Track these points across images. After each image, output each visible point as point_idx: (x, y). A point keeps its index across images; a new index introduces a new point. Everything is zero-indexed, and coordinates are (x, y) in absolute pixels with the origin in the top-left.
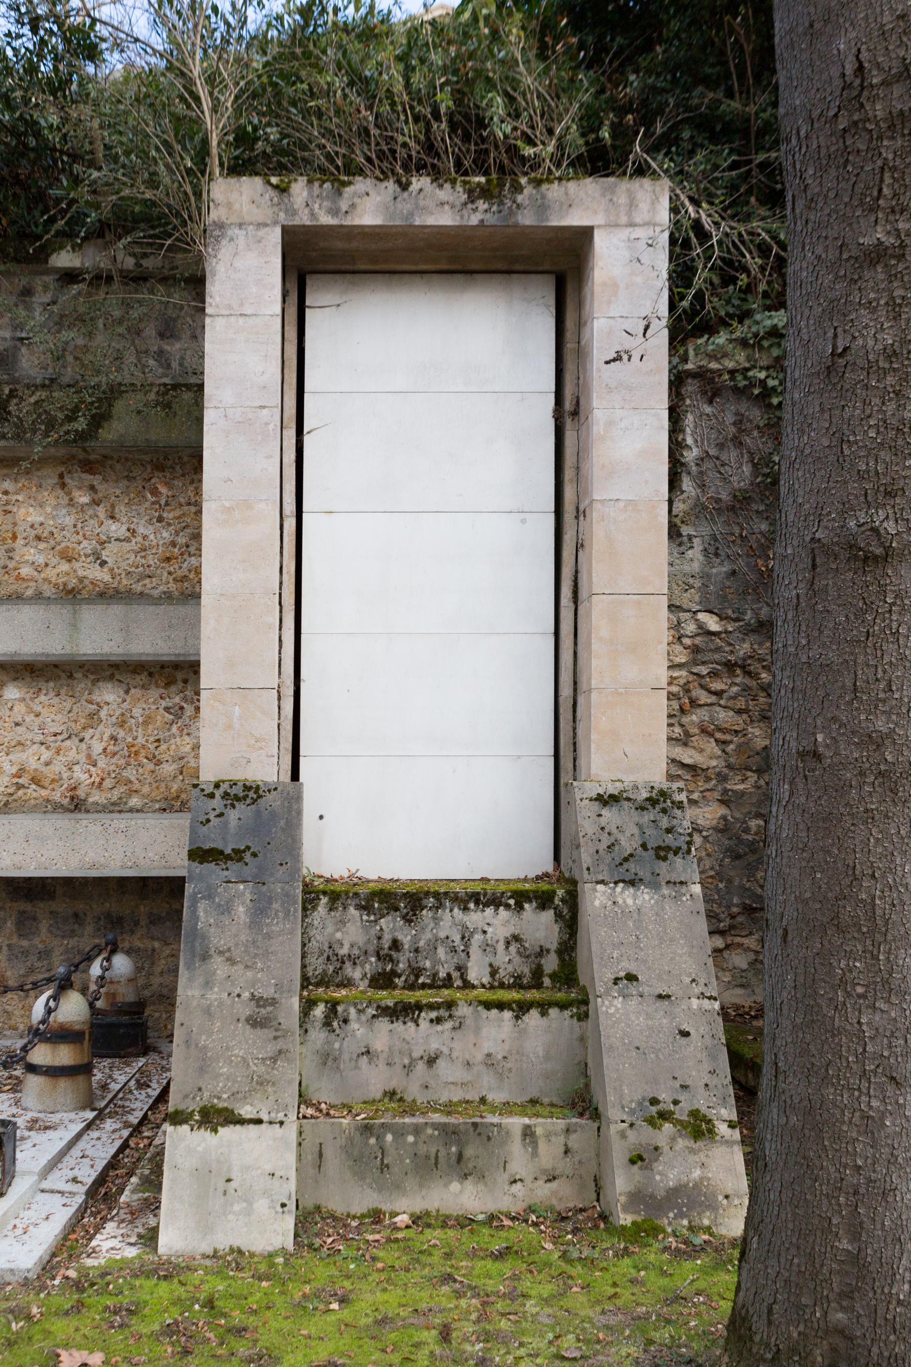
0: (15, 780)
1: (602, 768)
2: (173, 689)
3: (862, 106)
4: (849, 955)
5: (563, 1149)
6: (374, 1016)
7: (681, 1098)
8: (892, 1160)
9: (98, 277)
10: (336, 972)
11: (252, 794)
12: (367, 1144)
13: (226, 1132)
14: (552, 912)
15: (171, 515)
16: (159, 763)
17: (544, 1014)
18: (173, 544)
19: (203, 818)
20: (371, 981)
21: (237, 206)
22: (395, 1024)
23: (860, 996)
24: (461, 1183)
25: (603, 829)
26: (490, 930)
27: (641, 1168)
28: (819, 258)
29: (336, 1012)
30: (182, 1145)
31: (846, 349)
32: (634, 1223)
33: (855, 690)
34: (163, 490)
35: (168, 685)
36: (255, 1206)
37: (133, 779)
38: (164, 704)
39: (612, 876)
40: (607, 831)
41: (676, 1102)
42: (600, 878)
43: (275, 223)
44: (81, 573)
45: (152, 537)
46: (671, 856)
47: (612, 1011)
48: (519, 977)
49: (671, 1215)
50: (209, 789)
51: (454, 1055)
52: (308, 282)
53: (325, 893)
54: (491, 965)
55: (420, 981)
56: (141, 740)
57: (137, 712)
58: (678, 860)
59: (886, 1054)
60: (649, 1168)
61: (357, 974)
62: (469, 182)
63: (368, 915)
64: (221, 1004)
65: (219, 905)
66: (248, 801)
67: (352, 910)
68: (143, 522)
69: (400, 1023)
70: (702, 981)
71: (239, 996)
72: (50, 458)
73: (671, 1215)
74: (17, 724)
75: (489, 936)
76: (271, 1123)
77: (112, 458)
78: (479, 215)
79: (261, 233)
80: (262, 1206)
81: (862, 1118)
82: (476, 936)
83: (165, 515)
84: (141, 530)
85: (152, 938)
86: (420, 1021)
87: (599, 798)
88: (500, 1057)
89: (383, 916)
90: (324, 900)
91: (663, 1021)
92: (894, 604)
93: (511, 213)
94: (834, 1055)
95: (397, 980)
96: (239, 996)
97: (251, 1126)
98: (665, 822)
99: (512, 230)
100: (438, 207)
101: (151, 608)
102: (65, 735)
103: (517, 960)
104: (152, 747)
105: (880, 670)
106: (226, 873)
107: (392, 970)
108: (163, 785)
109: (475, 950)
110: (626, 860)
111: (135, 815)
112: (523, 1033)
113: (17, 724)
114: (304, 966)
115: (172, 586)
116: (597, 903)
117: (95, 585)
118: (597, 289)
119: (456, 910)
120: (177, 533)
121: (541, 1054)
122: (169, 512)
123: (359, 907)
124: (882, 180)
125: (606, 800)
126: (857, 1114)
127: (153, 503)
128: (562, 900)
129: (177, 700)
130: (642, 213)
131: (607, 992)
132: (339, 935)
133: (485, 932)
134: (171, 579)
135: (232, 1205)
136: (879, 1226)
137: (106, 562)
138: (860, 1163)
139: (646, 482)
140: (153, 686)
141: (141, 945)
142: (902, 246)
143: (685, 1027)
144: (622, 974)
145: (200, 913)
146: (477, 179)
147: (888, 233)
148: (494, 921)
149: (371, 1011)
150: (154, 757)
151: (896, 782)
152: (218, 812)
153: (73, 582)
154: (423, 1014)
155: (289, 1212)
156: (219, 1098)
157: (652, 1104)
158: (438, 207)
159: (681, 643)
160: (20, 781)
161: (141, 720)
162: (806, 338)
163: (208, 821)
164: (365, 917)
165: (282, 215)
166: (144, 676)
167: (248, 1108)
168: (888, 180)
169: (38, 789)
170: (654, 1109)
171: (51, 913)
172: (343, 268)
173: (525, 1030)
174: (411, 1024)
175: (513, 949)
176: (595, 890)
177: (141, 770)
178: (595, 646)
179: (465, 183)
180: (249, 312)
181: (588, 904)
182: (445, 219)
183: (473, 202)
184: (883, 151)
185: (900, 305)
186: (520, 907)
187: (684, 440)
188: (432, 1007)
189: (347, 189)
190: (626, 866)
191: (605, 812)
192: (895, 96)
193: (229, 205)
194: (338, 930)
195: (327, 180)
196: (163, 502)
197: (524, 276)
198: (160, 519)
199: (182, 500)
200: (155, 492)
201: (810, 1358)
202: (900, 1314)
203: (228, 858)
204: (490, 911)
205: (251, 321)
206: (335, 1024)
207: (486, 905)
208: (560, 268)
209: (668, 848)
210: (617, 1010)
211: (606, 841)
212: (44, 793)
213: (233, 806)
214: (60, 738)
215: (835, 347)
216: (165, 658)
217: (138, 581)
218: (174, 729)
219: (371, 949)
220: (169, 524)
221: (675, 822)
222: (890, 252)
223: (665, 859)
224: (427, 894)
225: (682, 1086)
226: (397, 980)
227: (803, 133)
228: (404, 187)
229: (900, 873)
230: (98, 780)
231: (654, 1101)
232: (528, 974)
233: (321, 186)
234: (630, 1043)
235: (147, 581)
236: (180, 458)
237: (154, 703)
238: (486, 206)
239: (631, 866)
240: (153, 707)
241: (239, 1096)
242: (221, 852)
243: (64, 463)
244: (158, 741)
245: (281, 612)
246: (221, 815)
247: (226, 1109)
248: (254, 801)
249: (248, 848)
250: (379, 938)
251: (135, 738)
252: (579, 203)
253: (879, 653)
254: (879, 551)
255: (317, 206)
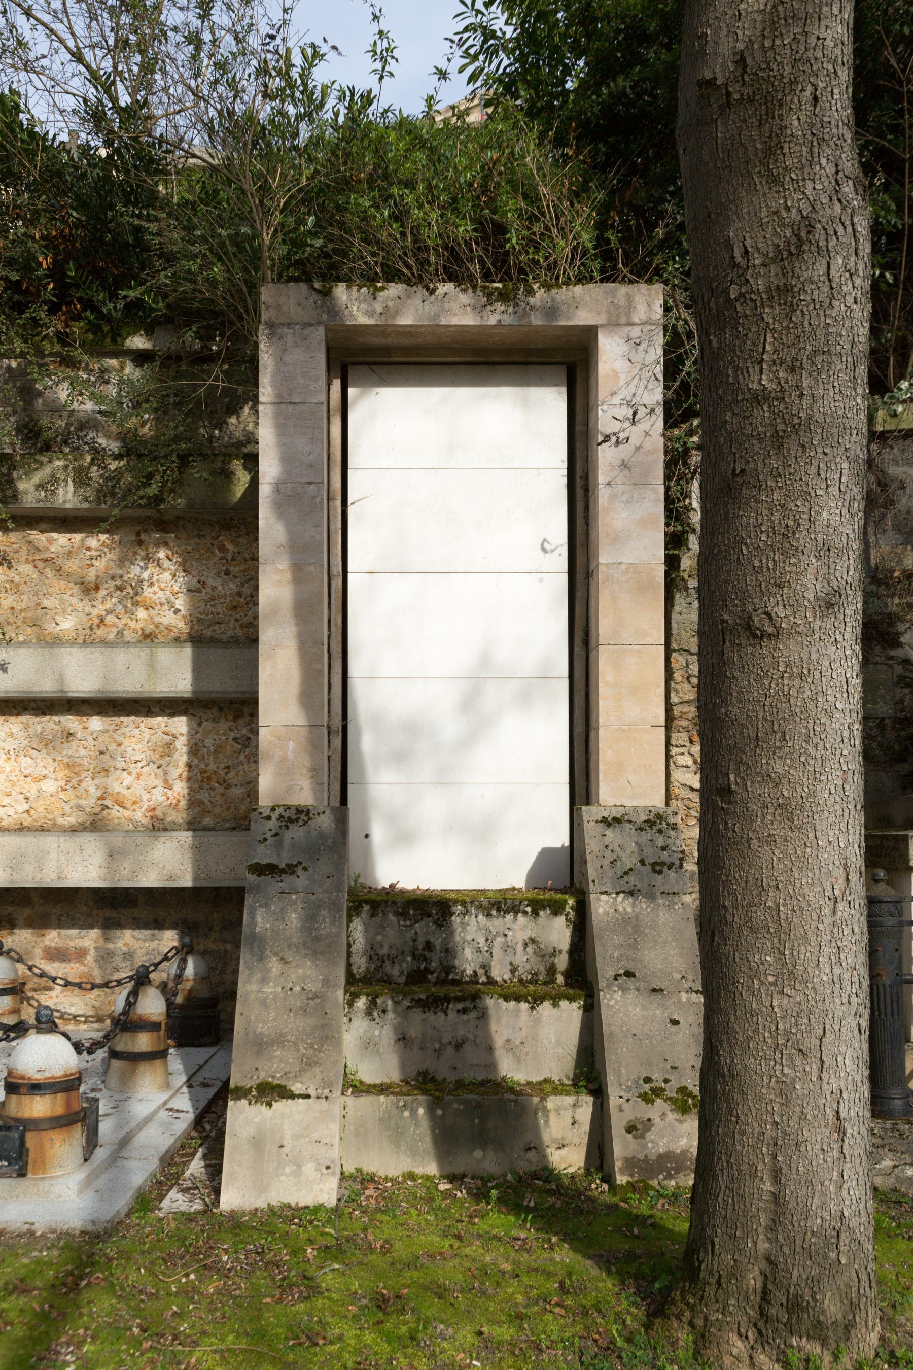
0: (100, 802)
1: (611, 794)
2: (241, 721)
3: (747, 281)
4: (761, 951)
5: (571, 1121)
6: (409, 1007)
7: (671, 1077)
8: (803, 1116)
9: (169, 358)
10: (377, 969)
11: (303, 817)
12: (402, 1117)
13: (281, 1106)
14: (563, 918)
15: (237, 569)
16: (229, 786)
17: (555, 1005)
18: (239, 594)
19: (261, 838)
20: (408, 977)
21: (285, 308)
22: (427, 1014)
23: (771, 984)
24: (483, 1150)
25: (606, 847)
26: (510, 933)
27: (635, 1137)
28: (721, 398)
29: (376, 1004)
30: (242, 1118)
31: (743, 471)
32: (628, 1182)
33: (757, 738)
34: (230, 546)
35: (236, 718)
36: (304, 1168)
37: (206, 801)
38: (232, 735)
39: (614, 887)
40: (610, 848)
41: (666, 1081)
42: (604, 889)
43: (319, 323)
44: (156, 619)
45: (220, 588)
46: (665, 869)
47: (612, 1002)
48: (536, 974)
49: (661, 1177)
50: (266, 812)
51: (479, 1041)
52: (350, 372)
53: (367, 902)
54: (511, 964)
55: (450, 977)
56: (212, 767)
57: (209, 742)
58: (672, 874)
59: (793, 1030)
60: (642, 1136)
61: (395, 972)
62: (488, 287)
63: (404, 920)
64: (276, 996)
65: (275, 913)
66: (300, 823)
67: (391, 917)
68: (212, 575)
69: (431, 1012)
70: (691, 978)
71: (291, 989)
72: (128, 518)
73: (661, 1177)
74: (102, 753)
75: (509, 938)
76: (318, 1098)
77: (183, 518)
78: (496, 316)
79: (307, 331)
80: (309, 1168)
81: (777, 1082)
82: (498, 939)
83: (232, 569)
84: (211, 582)
85: (225, 941)
86: (449, 1011)
87: (604, 820)
88: (518, 1043)
89: (417, 922)
90: (366, 908)
91: (658, 1012)
92: (785, 672)
93: (525, 314)
94: (753, 1031)
95: (430, 977)
96: (291, 989)
97: (301, 1100)
98: (660, 842)
99: (526, 329)
100: (457, 309)
101: (220, 651)
102: (144, 763)
103: (533, 959)
104: (222, 773)
105: (776, 724)
106: (281, 885)
107: (426, 968)
108: (233, 806)
109: (497, 951)
110: (626, 873)
111: (208, 833)
112: (537, 1021)
113: (102, 753)
114: (349, 965)
115: (239, 632)
116: (601, 911)
117: (171, 630)
118: (601, 380)
119: (480, 916)
120: (242, 585)
121: (553, 1040)
122: (235, 566)
123: (397, 914)
124: (765, 340)
125: (607, 822)
126: (773, 1080)
127: (221, 558)
128: (572, 908)
129: (244, 731)
130: (640, 313)
131: (609, 986)
132: (379, 938)
133: (505, 935)
134: (237, 625)
135: (283, 1168)
136: (794, 1171)
137: (179, 610)
138: (777, 1120)
139: (645, 548)
140: (223, 720)
141: (216, 948)
142: (782, 391)
143: (676, 1017)
144: (621, 971)
145: (259, 919)
146: (495, 285)
147: (771, 380)
148: (514, 926)
149: (406, 1003)
150: (225, 781)
151: (792, 813)
152: (273, 832)
153: (150, 628)
154: (451, 1006)
155: (333, 1173)
156: (273, 1077)
157: (645, 1082)
158: (457, 309)
159: (689, 682)
160: (105, 802)
161: (212, 749)
162: (713, 460)
163: (265, 840)
164: (402, 923)
165: (325, 316)
166: (214, 710)
167: (298, 1085)
168: (769, 339)
169: (121, 809)
170: (647, 1087)
171: (134, 919)
172: (381, 359)
173: (539, 1020)
174: (441, 1015)
175: (530, 949)
176: (599, 900)
177: (212, 793)
178: (602, 689)
179: (484, 288)
180: (297, 400)
181: (593, 911)
182: (469, 319)
183: (491, 304)
184: (765, 316)
185: (782, 437)
186: (535, 913)
187: (690, 504)
188: (458, 999)
189: (382, 293)
190: (626, 878)
191: (609, 832)
192: (772, 273)
193: (279, 307)
194: (378, 934)
195: (364, 285)
196: (229, 558)
197: (539, 367)
198: (227, 573)
199: (247, 556)
200: (222, 549)
201: (745, 1281)
202: (815, 1244)
203: (283, 871)
204: (509, 917)
205: (299, 408)
206: (375, 1014)
207: (507, 912)
208: (568, 362)
209: (663, 864)
210: (617, 1002)
211: (610, 857)
212: (126, 813)
213: (287, 827)
214: (139, 765)
215: (734, 470)
216: (233, 695)
217: (209, 627)
218: (242, 757)
219: (407, 950)
220: (236, 577)
221: (669, 841)
222: (773, 395)
223: (660, 872)
224: (456, 902)
225: (672, 1067)
226: (430, 977)
227: (706, 299)
228: (432, 292)
229: (798, 886)
230: (174, 802)
231: (648, 1080)
232: (544, 972)
233: (358, 291)
234: (628, 1030)
235: (217, 627)
236: (244, 518)
237: (224, 735)
238: (503, 308)
239: (631, 879)
240: (223, 738)
241: (291, 1075)
242: (276, 867)
243: (140, 523)
244: (228, 767)
245: (329, 659)
246: (276, 835)
247: (279, 1086)
248: (305, 823)
249: (300, 863)
250: (414, 940)
251: (207, 765)
252: (584, 305)
253: (775, 711)
254: (770, 630)
255: (355, 308)
